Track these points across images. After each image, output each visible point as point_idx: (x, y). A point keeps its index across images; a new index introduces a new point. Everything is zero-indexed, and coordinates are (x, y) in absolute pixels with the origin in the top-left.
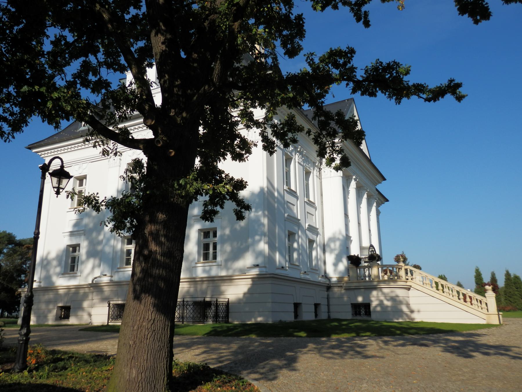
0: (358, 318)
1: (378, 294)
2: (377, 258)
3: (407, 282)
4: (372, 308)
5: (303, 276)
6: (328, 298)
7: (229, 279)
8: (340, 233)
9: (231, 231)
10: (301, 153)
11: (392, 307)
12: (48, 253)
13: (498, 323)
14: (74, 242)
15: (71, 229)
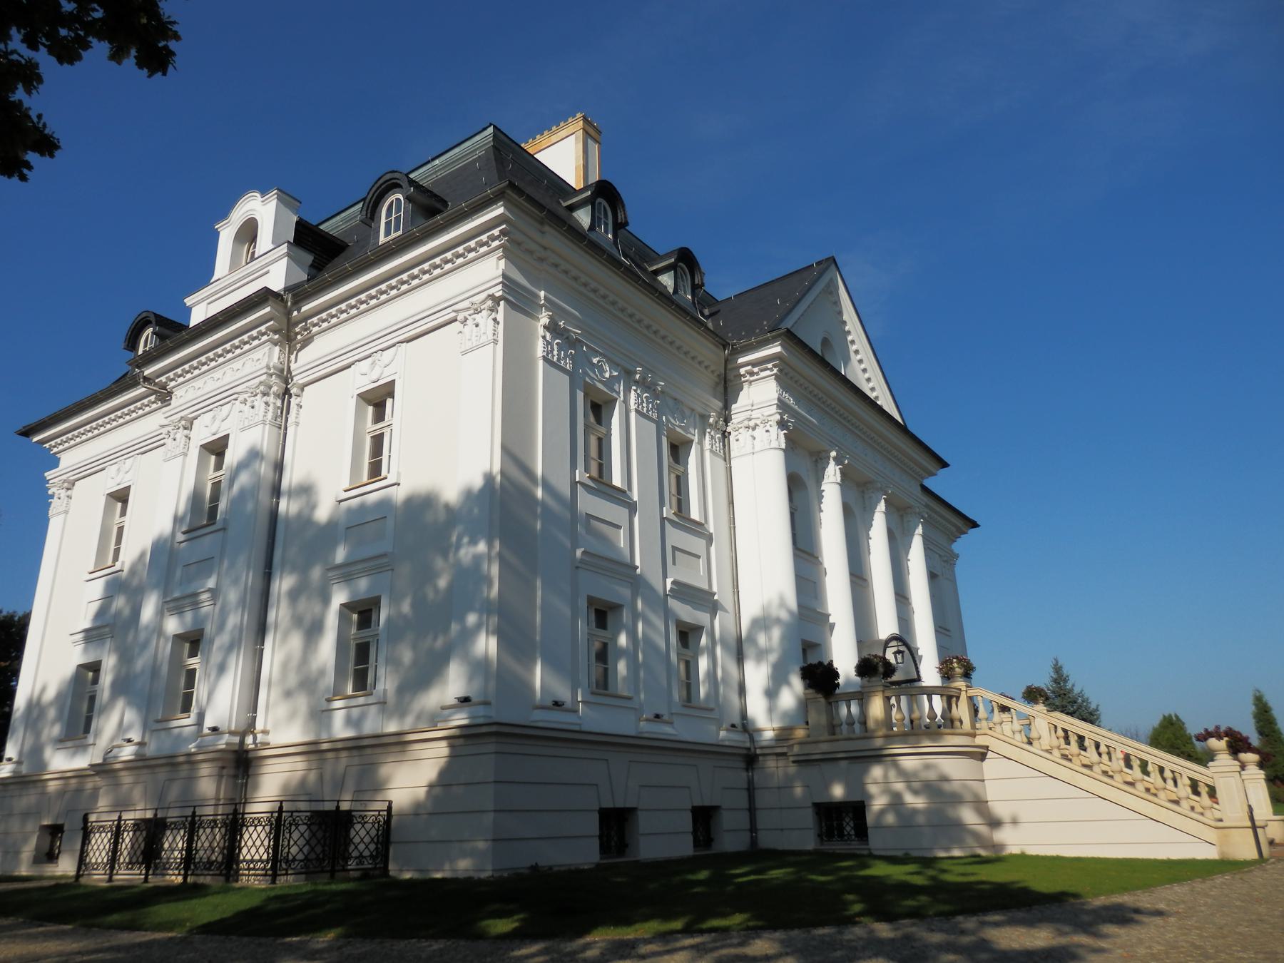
0: (837, 847)
1: (886, 776)
2: (881, 669)
3: (974, 736)
4: (870, 819)
5: (646, 728)
6: (751, 789)
7: (397, 744)
8: (782, 604)
9: (414, 606)
10: (645, 385)
11: (927, 812)
12: (43, 690)
13: (1254, 855)
14: (90, 658)
15: (87, 625)
